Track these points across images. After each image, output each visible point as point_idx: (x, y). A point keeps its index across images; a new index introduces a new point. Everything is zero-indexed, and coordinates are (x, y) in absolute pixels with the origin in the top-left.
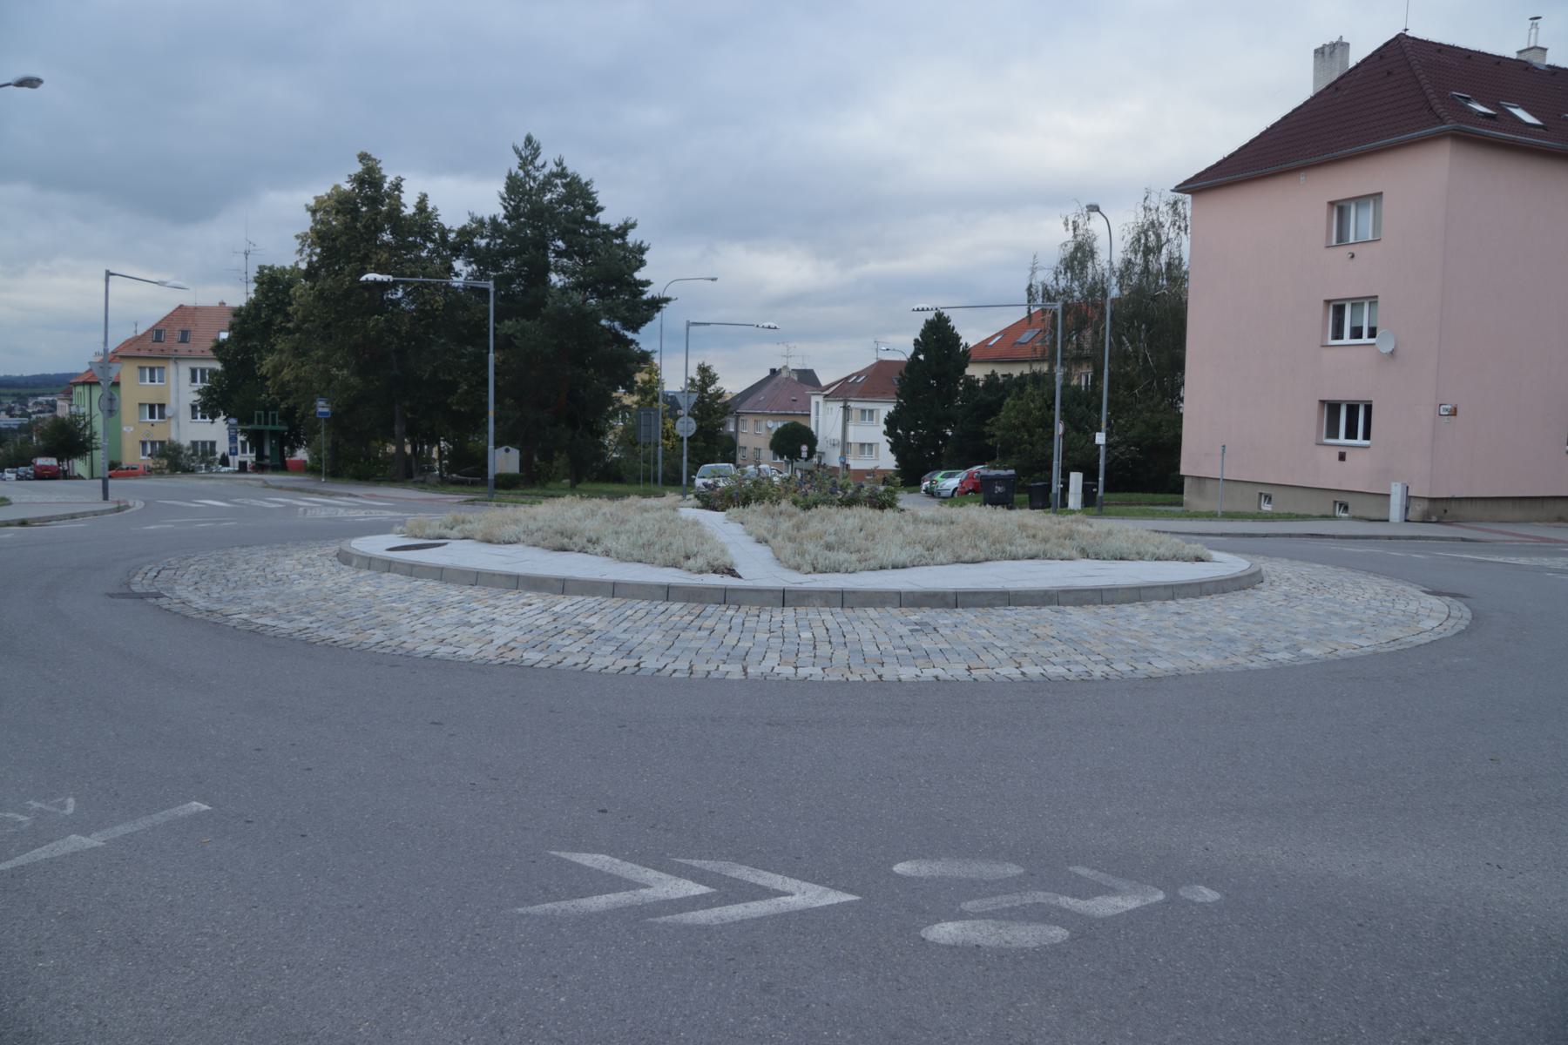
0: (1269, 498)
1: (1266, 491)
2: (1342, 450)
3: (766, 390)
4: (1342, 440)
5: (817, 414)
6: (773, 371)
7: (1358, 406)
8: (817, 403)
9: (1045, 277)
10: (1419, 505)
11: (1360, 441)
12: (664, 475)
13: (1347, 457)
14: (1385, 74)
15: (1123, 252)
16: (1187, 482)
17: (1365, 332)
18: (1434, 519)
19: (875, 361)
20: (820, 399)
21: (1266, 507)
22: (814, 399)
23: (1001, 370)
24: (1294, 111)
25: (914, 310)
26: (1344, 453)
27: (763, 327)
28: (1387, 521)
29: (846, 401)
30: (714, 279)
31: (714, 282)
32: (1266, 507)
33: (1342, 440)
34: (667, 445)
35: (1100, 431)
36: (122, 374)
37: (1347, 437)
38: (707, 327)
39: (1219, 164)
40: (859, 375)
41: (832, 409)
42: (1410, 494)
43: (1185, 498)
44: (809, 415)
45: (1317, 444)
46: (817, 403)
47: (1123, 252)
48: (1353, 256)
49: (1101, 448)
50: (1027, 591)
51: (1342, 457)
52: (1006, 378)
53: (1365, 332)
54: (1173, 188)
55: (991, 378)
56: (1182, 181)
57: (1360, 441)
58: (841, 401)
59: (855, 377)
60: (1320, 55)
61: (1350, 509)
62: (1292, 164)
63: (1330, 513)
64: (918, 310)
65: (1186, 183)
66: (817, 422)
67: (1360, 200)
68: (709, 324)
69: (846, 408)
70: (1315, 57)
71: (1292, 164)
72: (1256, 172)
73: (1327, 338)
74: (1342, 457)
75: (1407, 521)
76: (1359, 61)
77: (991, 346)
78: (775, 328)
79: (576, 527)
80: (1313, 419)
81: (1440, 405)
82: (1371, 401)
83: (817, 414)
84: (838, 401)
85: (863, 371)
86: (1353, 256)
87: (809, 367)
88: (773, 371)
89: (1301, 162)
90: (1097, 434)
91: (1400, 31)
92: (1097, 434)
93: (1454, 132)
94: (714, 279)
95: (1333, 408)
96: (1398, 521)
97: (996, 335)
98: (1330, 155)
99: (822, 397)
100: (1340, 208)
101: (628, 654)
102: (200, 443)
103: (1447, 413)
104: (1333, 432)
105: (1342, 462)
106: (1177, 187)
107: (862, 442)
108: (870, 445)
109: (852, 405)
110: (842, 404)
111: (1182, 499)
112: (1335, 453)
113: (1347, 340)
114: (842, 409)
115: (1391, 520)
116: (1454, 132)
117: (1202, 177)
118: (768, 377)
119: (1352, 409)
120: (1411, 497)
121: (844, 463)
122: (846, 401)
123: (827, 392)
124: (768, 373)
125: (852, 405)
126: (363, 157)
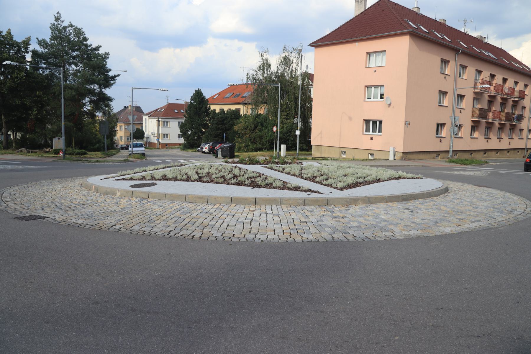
0: (344, 152)
2: (372, 136)
3: (123, 114)
4: (371, 133)
5: (146, 123)
6: (125, 107)
7: (377, 121)
8: (146, 119)
9: (251, 72)
10: (399, 155)
11: (377, 133)
12: (107, 146)
13: (374, 139)
15: (105, 53)
16: (313, 147)
18: (403, 159)
19: (167, 104)
20: (147, 117)
21: (343, 156)
22: (144, 118)
23: (226, 108)
24: (350, 21)
27: (163, 90)
28: (389, 160)
29: (158, 118)
30: (126, 71)
31: (126, 72)
32: (343, 156)
33: (371, 133)
34: (284, 140)
35: (297, 130)
37: (373, 132)
38: (140, 90)
39: (325, 37)
40: (161, 108)
41: (151, 121)
43: (312, 153)
44: (142, 124)
45: (363, 134)
46: (146, 119)
47: (105, 53)
48: (375, 71)
49: (298, 136)
51: (372, 139)
52: (91, 103)
54: (309, 44)
55: (222, 110)
57: (377, 133)
58: (157, 118)
59: (160, 110)
60: (357, 2)
62: (360, 38)
65: (313, 43)
66: (146, 126)
68: (141, 88)
69: (159, 121)
70: (355, 3)
71: (360, 38)
72: (341, 41)
73: (365, 99)
74: (372, 139)
75: (395, 160)
76: (371, 6)
77: (215, 99)
78: (167, 91)
79: (377, 168)
80: (361, 125)
81: (406, 122)
82: (382, 120)
83: (146, 123)
84: (156, 118)
85: (163, 107)
86: (375, 71)
87: (138, 106)
88: (125, 107)
89: (357, 39)
90: (296, 131)
92: (296, 131)
93: (412, 32)
94: (126, 71)
95: (368, 121)
96: (392, 160)
97: (216, 94)
98: (368, 37)
99: (148, 117)
100: (369, 54)
103: (407, 124)
104: (367, 130)
105: (372, 140)
106: (310, 44)
107: (164, 133)
108: (167, 135)
109: (160, 119)
110: (157, 119)
111: (312, 153)
112: (369, 137)
114: (157, 121)
115: (390, 160)
116: (412, 32)
117: (319, 41)
118: (123, 109)
119: (375, 122)
120: (396, 152)
121: (158, 141)
122: (158, 118)
123: (149, 115)
124: (123, 108)
125: (160, 119)
126: (70, 22)
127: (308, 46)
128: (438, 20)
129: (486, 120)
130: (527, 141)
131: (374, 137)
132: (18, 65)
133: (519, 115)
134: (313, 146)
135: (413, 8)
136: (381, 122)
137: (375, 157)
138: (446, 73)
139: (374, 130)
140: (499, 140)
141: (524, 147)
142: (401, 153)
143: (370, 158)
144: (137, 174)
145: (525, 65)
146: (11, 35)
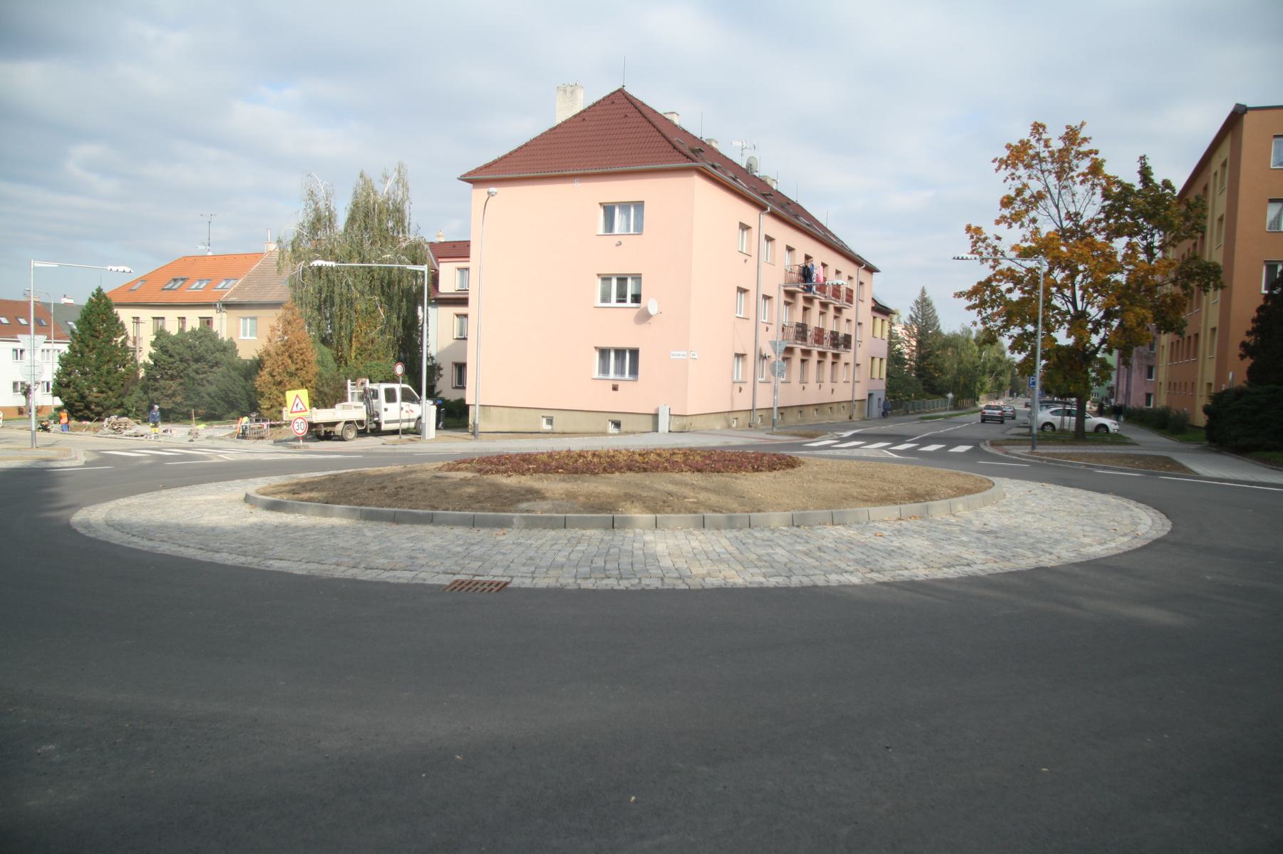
1: (617, 418)
2: (615, 383)
14: (623, 115)
17: (629, 298)
24: (551, 130)
25: (954, 258)
26: (19, 414)
36: (1122, 247)
42: (671, 413)
50: (1218, 452)
51: (615, 388)
53: (629, 298)
56: (473, 168)
61: (622, 427)
63: (600, 429)
64: (958, 258)
67: (625, 206)
91: (620, 87)
101: (986, 563)
102: (19, 383)
105: (614, 392)
113: (629, 303)
119: (620, 353)
127: (459, 179)
128: (704, 140)
129: (805, 345)
130: (854, 385)
131: (621, 385)
132: (334, 266)
133: (1121, 361)
134: (470, 407)
135: (665, 113)
136: (635, 353)
137: (558, 427)
138: (744, 252)
139: (620, 370)
140: (818, 385)
141: (850, 399)
142: (651, 416)
143: (545, 427)
144: (765, 477)
145: (829, 232)
146: (1162, 332)
